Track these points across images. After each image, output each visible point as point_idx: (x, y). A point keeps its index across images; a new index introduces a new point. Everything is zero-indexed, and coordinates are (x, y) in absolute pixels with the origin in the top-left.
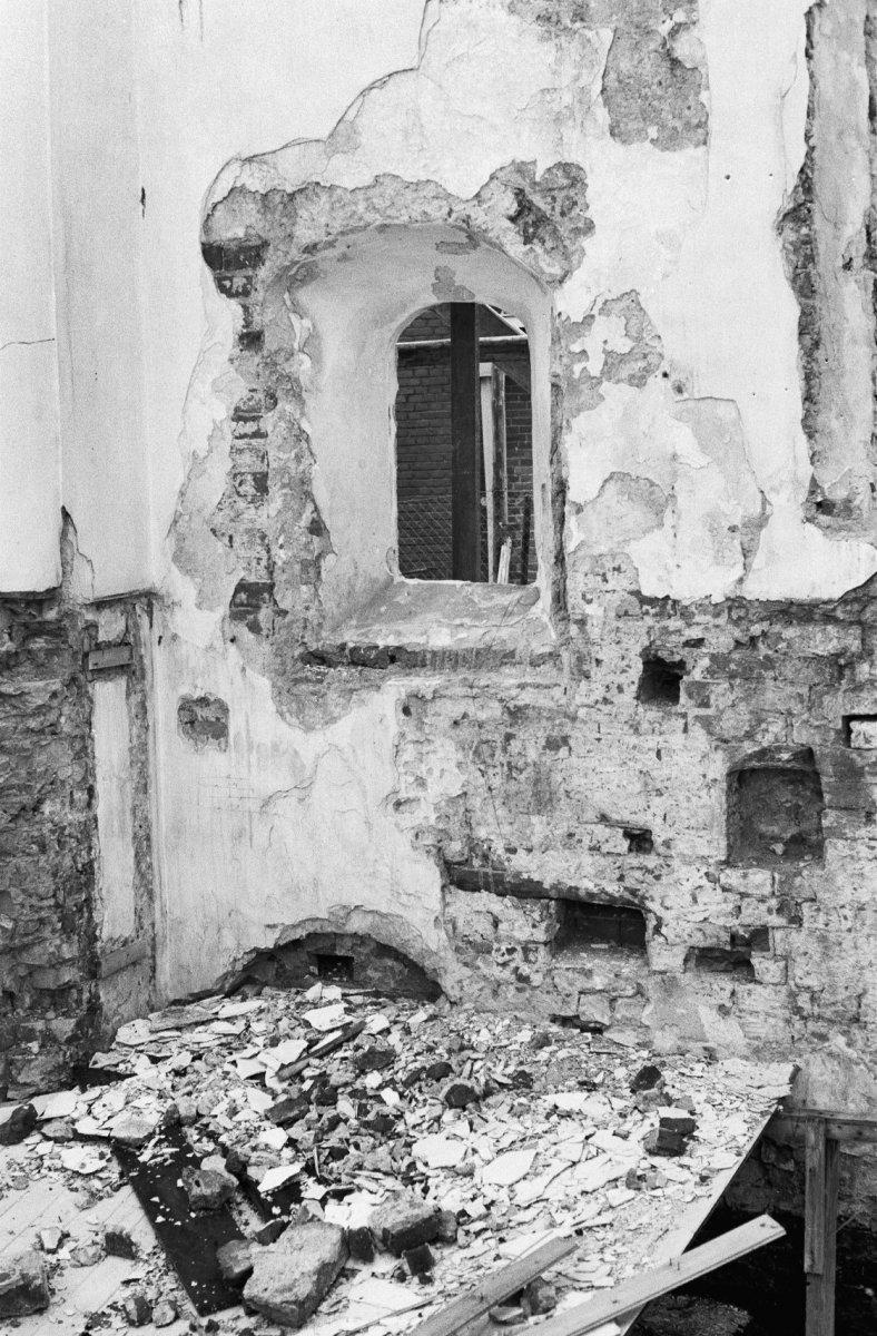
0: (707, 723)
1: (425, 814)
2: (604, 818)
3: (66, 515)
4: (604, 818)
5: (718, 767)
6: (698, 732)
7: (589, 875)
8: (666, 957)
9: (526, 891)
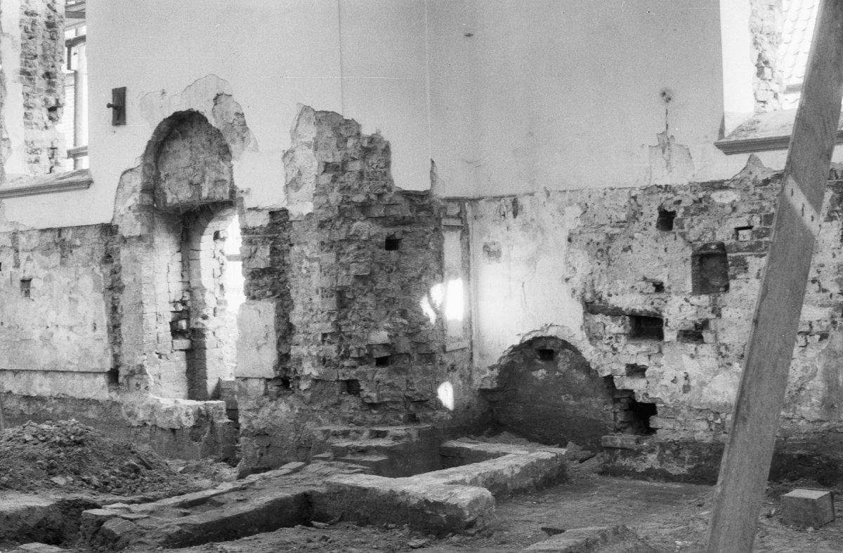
0: (683, 235)
1: (577, 282)
2: (645, 279)
3: (433, 162)
4: (645, 279)
5: (689, 253)
6: (679, 238)
7: (635, 302)
8: (669, 335)
9: (616, 313)
